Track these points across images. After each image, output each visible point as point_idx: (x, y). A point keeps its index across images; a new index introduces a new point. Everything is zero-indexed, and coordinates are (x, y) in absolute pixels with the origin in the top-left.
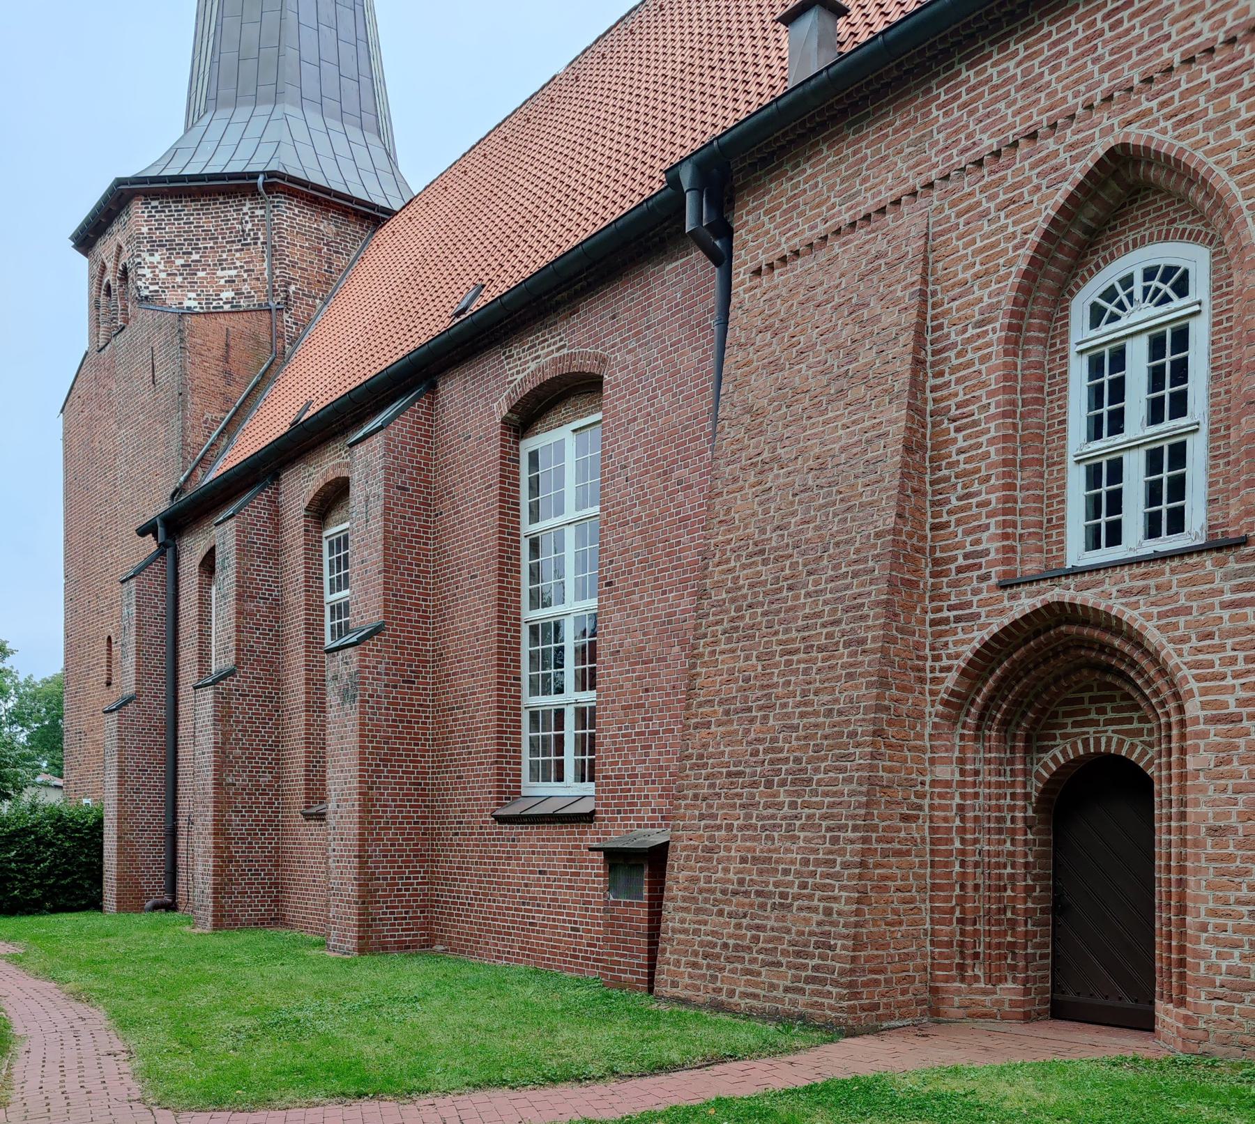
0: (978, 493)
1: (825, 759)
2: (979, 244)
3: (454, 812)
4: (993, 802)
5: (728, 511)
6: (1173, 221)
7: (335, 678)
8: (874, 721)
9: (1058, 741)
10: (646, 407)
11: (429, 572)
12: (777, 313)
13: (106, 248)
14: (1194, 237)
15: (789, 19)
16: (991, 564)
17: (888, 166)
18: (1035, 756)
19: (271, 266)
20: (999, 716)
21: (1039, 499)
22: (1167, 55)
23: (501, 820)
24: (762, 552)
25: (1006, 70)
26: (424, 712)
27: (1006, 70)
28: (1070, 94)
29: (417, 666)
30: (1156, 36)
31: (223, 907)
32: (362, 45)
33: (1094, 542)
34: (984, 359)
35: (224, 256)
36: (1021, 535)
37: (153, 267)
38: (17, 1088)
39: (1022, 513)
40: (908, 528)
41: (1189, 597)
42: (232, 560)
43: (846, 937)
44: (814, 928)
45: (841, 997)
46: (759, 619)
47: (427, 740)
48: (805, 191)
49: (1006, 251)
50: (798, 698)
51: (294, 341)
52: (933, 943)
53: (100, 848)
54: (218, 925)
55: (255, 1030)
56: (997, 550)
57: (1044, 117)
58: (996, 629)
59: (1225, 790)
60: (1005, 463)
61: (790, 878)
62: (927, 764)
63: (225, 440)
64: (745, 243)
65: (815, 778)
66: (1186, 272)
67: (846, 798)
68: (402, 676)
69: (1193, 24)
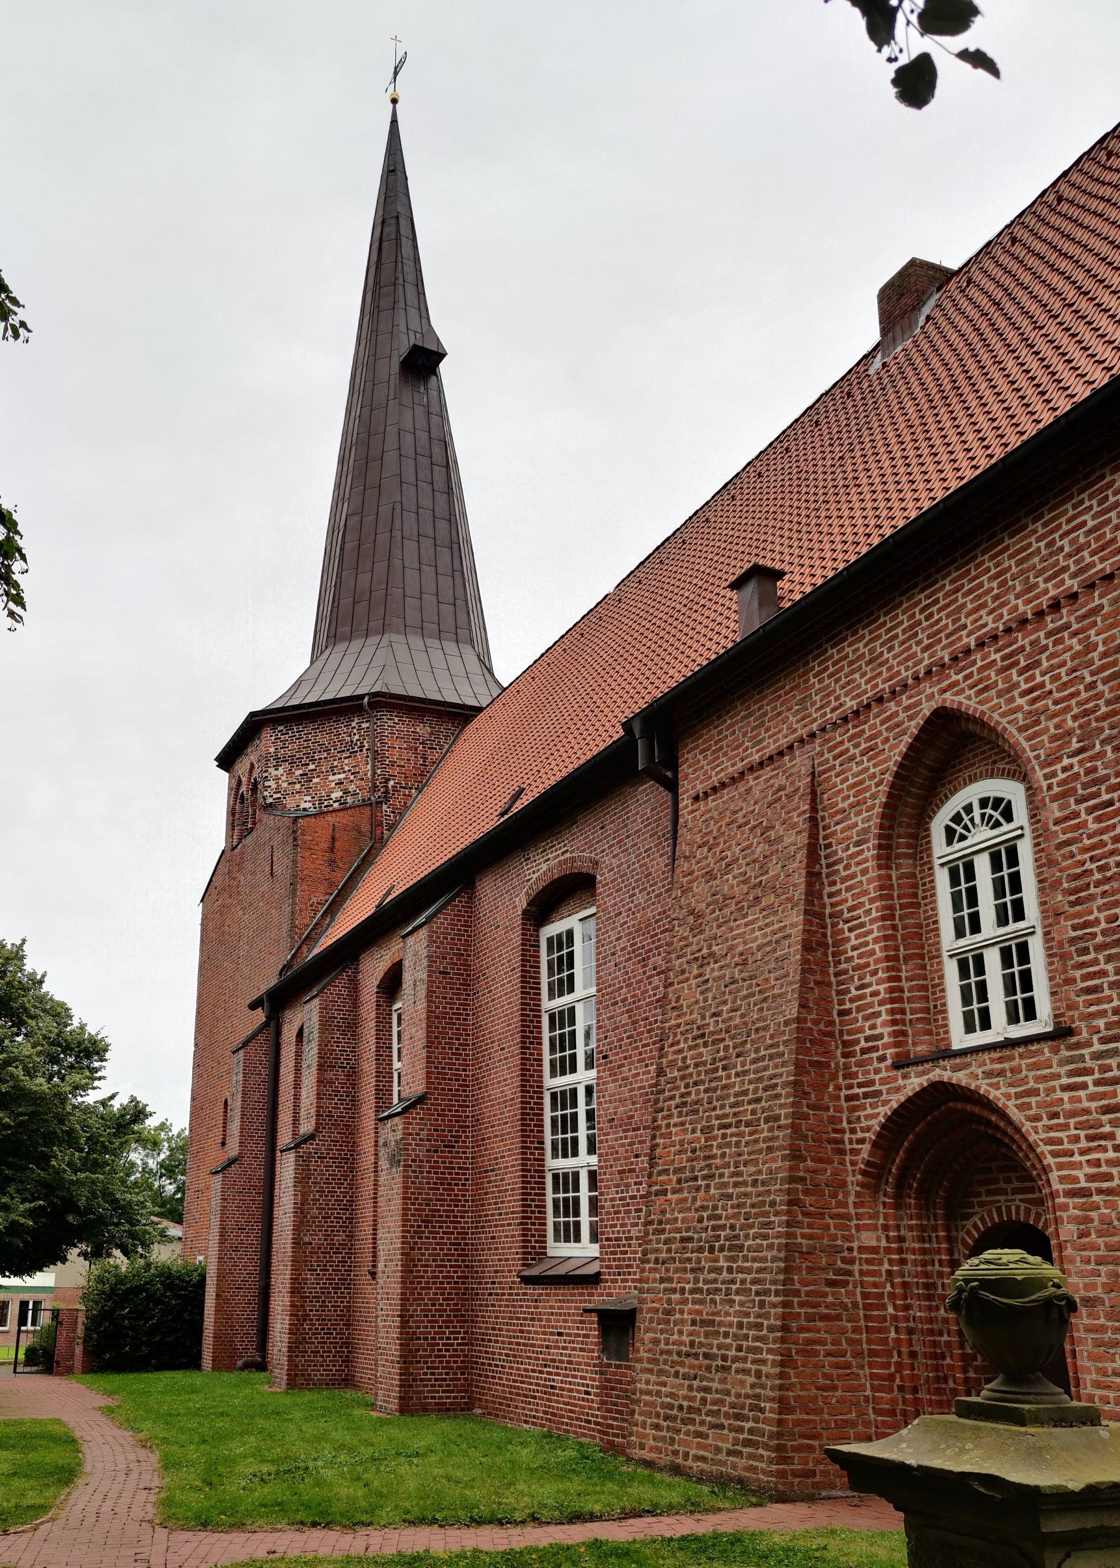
0: (869, 985)
1: (752, 1226)
2: (851, 781)
3: (489, 1272)
4: (919, 1269)
5: (678, 999)
6: (995, 762)
7: (385, 1144)
8: (789, 1192)
9: (977, 1209)
10: (628, 903)
11: (468, 1045)
12: (711, 832)
13: (242, 767)
14: (1012, 775)
15: (736, 585)
16: (886, 1046)
17: (782, 720)
18: (959, 1223)
19: (374, 766)
20: (915, 1185)
21: (925, 988)
22: (965, 640)
23: (527, 1280)
24: (703, 1036)
25: (858, 649)
26: (464, 1174)
27: (858, 649)
28: (902, 668)
29: (457, 1131)
30: (957, 625)
31: (297, 1366)
32: (458, 574)
33: (969, 1028)
34: (864, 872)
35: (335, 763)
36: (911, 1020)
37: (277, 779)
38: (68, 1509)
39: (910, 1000)
40: (814, 1016)
41: (1037, 1079)
42: (316, 1035)
43: (772, 1400)
44: (748, 1390)
45: (771, 1461)
46: (702, 1095)
47: (467, 1201)
48: (726, 736)
49: (869, 787)
50: (732, 1169)
51: (392, 827)
52: (876, 1412)
53: (202, 1303)
54: (292, 1384)
55: (270, 1475)
56: (889, 1035)
57: (886, 685)
58: (895, 1106)
59: (1088, 1262)
60: (888, 959)
61: (729, 1341)
62: (853, 1231)
63: (328, 919)
64: (687, 776)
65: (746, 1244)
66: (1009, 802)
67: (769, 1264)
68: (443, 1141)
69: (981, 617)
